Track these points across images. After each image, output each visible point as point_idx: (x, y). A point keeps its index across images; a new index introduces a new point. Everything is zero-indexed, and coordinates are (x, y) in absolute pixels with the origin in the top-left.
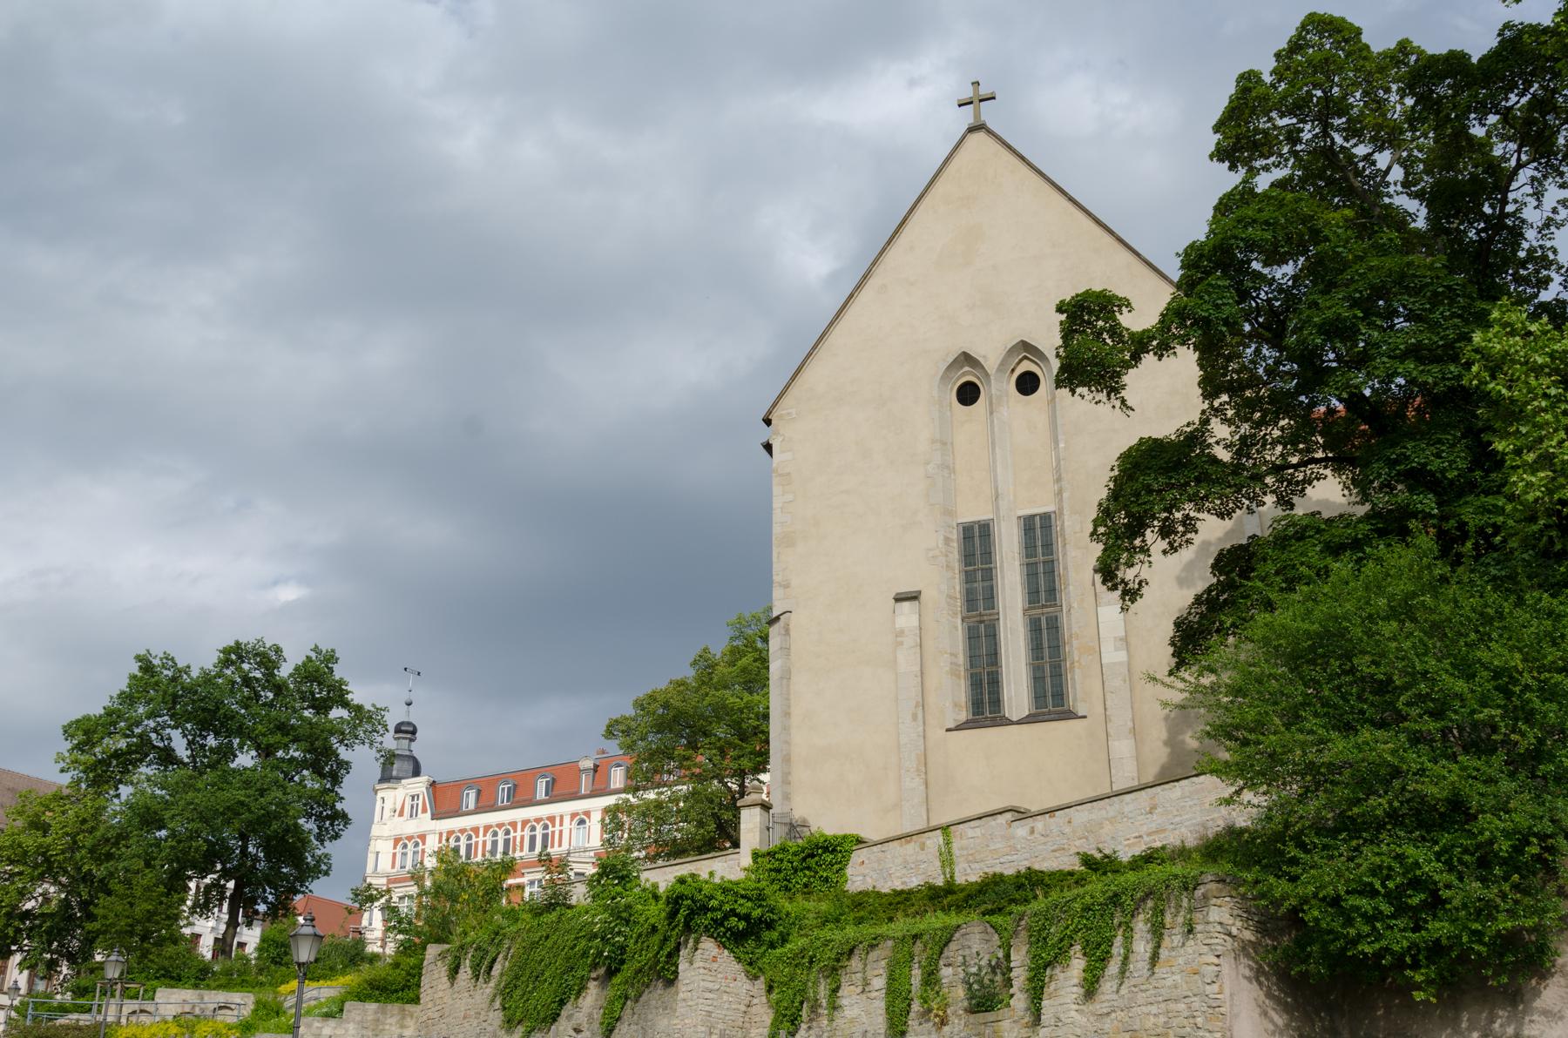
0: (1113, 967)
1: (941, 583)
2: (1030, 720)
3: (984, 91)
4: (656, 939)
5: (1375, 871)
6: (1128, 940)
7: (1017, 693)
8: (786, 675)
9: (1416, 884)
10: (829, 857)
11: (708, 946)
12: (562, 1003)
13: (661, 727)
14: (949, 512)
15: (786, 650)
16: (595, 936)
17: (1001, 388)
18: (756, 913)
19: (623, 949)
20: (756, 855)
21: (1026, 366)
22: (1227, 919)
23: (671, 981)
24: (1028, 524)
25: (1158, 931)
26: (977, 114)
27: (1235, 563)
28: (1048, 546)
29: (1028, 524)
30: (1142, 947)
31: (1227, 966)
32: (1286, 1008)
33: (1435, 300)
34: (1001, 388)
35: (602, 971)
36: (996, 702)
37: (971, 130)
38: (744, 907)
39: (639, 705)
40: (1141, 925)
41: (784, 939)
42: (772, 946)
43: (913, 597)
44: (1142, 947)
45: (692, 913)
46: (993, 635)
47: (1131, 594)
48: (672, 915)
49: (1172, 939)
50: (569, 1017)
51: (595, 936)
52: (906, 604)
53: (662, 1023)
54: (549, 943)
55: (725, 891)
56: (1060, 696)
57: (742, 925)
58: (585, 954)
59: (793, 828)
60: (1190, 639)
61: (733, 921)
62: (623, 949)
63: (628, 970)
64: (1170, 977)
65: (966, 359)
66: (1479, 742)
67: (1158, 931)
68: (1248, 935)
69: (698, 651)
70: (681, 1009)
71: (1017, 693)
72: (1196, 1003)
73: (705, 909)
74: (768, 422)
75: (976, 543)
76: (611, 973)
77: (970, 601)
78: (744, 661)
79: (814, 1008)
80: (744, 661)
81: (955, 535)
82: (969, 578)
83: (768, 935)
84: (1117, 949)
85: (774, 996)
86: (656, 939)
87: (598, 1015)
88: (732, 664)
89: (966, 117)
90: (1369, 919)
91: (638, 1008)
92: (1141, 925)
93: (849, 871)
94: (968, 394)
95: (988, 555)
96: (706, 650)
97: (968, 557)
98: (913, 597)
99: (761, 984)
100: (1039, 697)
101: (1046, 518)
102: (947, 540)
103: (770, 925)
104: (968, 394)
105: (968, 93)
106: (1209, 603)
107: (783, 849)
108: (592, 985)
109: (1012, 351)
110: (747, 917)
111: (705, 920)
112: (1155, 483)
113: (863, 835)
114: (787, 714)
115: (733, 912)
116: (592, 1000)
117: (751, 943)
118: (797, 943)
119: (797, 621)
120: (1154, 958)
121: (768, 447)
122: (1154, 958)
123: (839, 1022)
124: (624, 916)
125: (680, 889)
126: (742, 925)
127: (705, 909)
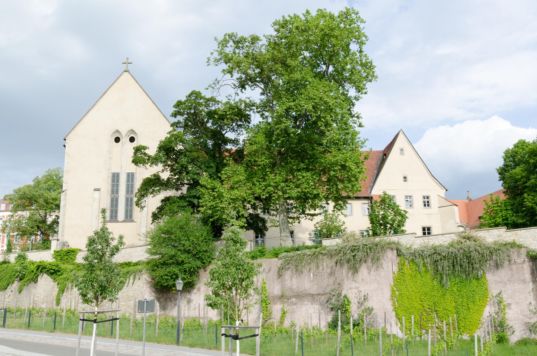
0: (126, 284)
1: (106, 187)
2: (123, 221)
3: (129, 61)
4: (34, 273)
5: (168, 272)
6: (129, 280)
7: (121, 215)
8: (65, 206)
9: (175, 274)
10: (73, 253)
11: (45, 275)
12: (8, 285)
13: (21, 198)
14: (109, 170)
15: (65, 199)
16: (18, 272)
17: (125, 140)
18: (56, 269)
19: (25, 275)
20: (55, 251)
21: (132, 135)
22: (146, 277)
23: (36, 282)
24: (128, 174)
25: (134, 279)
26: (127, 67)
27: (167, 200)
28: (133, 180)
29: (128, 174)
30: (131, 281)
31: (145, 286)
32: (154, 292)
33: (202, 164)
34: (125, 140)
35: (18, 279)
36: (116, 216)
37: (125, 71)
38: (54, 268)
39: (15, 191)
40: (132, 277)
41: (62, 274)
42: (59, 275)
43: (98, 190)
44: (131, 281)
45: (42, 269)
46: (117, 200)
47: (142, 208)
48: (38, 269)
49: (137, 280)
50: (10, 288)
51: (18, 272)
52: (97, 192)
53: (33, 291)
54: (5, 272)
55: (50, 264)
56: (131, 216)
57: (53, 271)
58: (14, 275)
59: (64, 244)
60: (155, 217)
61: (51, 271)
62: (25, 275)
63: (26, 279)
64: (135, 287)
65: (132, 131)
66: (188, 252)
67: (134, 279)
68: (150, 280)
69: (35, 177)
70: (38, 288)
71: (121, 215)
72: (139, 291)
73: (45, 268)
74: (65, 140)
75: (115, 177)
76: (21, 279)
77: (113, 192)
78: (49, 183)
79: (68, 289)
80: (49, 183)
81: (110, 175)
82: (113, 186)
83: (58, 273)
84: (127, 281)
85: (59, 286)
86: (34, 273)
87: (17, 288)
88: (45, 183)
89: (124, 67)
90: (166, 280)
91: (28, 287)
92: (132, 277)
93: (77, 257)
94: (117, 140)
95: (118, 181)
96: (37, 177)
97: (113, 181)
98: (98, 190)
99: (56, 283)
100: (126, 216)
101: (133, 174)
102: (108, 177)
103: (59, 271)
104: (117, 140)
105: (125, 61)
106: (160, 209)
107: (62, 251)
108: (16, 282)
109: (129, 131)
110: (54, 270)
111: (45, 270)
112: (152, 184)
113: (81, 249)
114: (64, 215)
115: (51, 269)
116: (16, 285)
117: (54, 275)
118: (65, 275)
119: (68, 192)
120: (133, 283)
121: (65, 146)
122: (133, 283)
123: (73, 292)
124: (25, 268)
125: (40, 264)
126: (53, 271)
127: (45, 268)
